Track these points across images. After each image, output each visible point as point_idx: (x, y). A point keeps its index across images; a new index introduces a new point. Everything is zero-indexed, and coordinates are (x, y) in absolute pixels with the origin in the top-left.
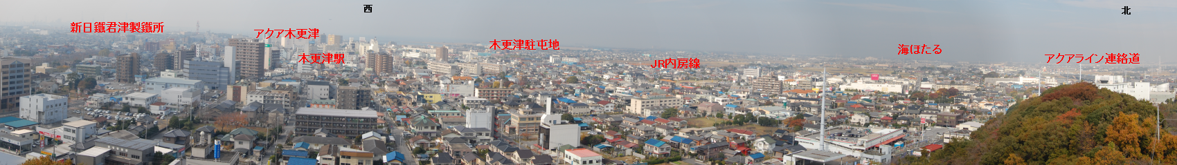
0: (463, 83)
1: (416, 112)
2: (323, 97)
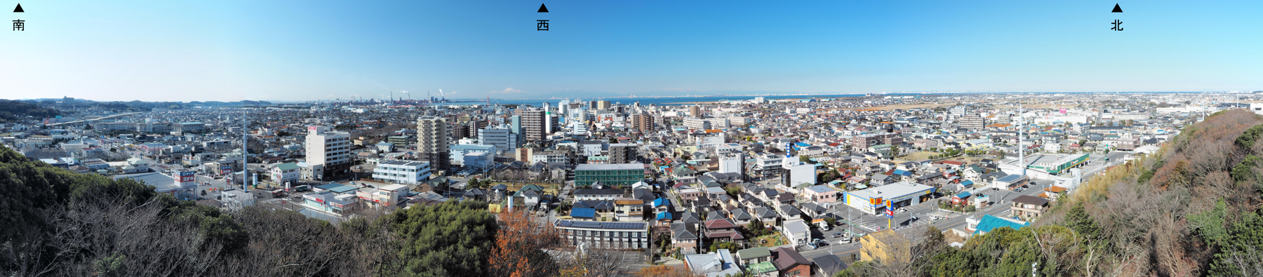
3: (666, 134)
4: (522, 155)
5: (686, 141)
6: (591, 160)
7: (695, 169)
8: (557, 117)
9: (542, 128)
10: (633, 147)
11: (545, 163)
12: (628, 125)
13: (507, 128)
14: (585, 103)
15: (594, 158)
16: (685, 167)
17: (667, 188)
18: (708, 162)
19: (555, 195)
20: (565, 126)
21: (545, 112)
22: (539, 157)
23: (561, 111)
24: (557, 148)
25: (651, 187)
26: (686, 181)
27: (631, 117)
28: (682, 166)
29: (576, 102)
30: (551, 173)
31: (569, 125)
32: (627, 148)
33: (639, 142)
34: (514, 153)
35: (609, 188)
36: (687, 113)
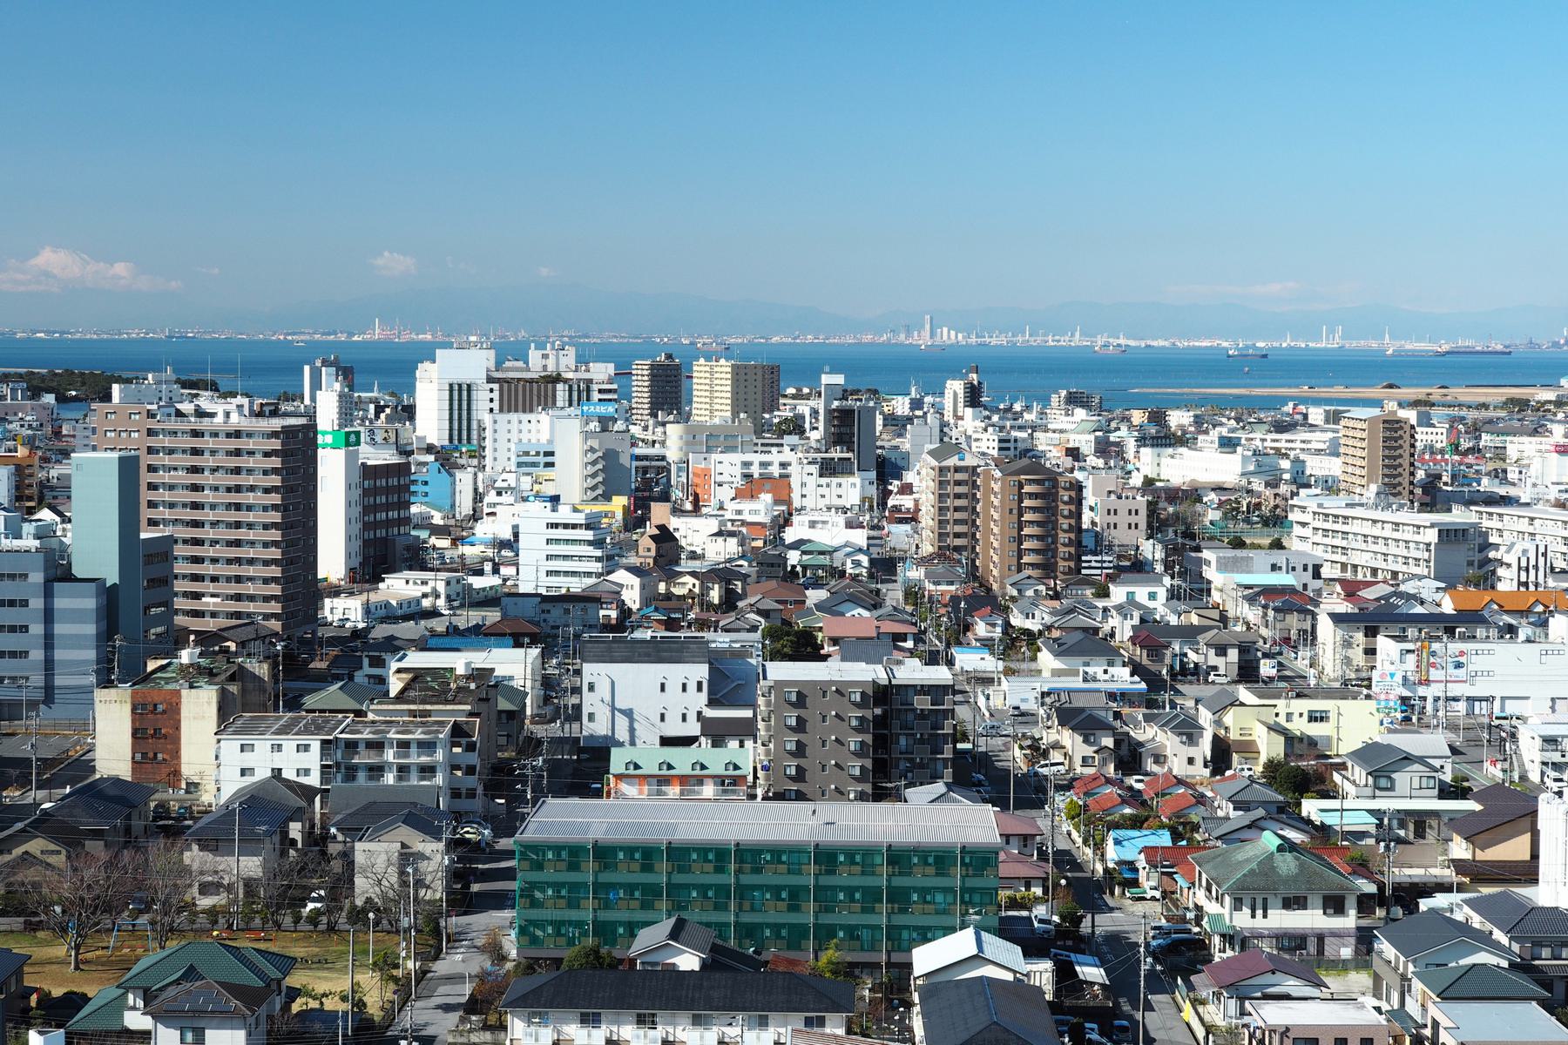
0: (1511, 630)
1: (1226, 809)
2: (675, 729)
3: (1161, 608)
4: (137, 734)
5: (1300, 662)
6: (634, 774)
7: (1362, 867)
8: (403, 470)
9: (286, 544)
10: (924, 690)
11: (308, 793)
12: (898, 534)
13: (29, 542)
14: (601, 372)
15: (651, 757)
16: (1287, 846)
17: (1159, 984)
18: (1461, 824)
19: (374, 1008)
20: (457, 532)
21: (310, 430)
22: (263, 745)
23: (430, 424)
24: (395, 685)
25: (1042, 973)
26: (1293, 942)
27: (921, 479)
28: (1269, 841)
29: (537, 363)
30: (347, 857)
31: (485, 529)
32: (883, 694)
33: (969, 659)
34: (86, 726)
35: (754, 964)
36: (1317, 467)
